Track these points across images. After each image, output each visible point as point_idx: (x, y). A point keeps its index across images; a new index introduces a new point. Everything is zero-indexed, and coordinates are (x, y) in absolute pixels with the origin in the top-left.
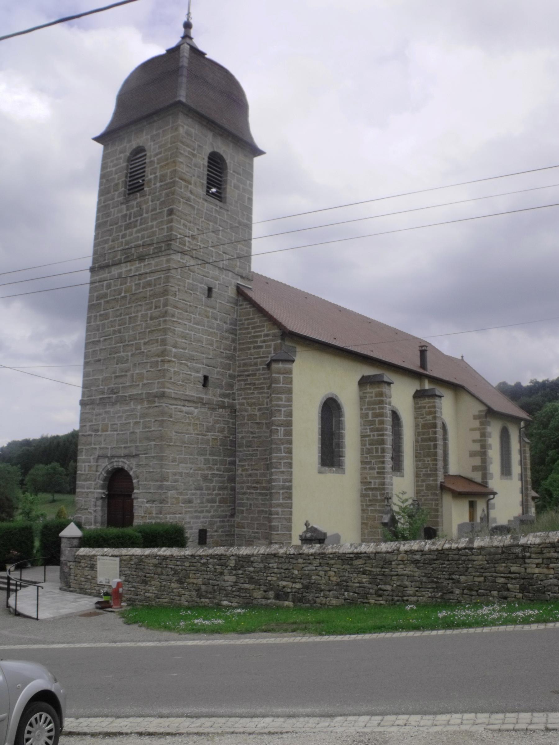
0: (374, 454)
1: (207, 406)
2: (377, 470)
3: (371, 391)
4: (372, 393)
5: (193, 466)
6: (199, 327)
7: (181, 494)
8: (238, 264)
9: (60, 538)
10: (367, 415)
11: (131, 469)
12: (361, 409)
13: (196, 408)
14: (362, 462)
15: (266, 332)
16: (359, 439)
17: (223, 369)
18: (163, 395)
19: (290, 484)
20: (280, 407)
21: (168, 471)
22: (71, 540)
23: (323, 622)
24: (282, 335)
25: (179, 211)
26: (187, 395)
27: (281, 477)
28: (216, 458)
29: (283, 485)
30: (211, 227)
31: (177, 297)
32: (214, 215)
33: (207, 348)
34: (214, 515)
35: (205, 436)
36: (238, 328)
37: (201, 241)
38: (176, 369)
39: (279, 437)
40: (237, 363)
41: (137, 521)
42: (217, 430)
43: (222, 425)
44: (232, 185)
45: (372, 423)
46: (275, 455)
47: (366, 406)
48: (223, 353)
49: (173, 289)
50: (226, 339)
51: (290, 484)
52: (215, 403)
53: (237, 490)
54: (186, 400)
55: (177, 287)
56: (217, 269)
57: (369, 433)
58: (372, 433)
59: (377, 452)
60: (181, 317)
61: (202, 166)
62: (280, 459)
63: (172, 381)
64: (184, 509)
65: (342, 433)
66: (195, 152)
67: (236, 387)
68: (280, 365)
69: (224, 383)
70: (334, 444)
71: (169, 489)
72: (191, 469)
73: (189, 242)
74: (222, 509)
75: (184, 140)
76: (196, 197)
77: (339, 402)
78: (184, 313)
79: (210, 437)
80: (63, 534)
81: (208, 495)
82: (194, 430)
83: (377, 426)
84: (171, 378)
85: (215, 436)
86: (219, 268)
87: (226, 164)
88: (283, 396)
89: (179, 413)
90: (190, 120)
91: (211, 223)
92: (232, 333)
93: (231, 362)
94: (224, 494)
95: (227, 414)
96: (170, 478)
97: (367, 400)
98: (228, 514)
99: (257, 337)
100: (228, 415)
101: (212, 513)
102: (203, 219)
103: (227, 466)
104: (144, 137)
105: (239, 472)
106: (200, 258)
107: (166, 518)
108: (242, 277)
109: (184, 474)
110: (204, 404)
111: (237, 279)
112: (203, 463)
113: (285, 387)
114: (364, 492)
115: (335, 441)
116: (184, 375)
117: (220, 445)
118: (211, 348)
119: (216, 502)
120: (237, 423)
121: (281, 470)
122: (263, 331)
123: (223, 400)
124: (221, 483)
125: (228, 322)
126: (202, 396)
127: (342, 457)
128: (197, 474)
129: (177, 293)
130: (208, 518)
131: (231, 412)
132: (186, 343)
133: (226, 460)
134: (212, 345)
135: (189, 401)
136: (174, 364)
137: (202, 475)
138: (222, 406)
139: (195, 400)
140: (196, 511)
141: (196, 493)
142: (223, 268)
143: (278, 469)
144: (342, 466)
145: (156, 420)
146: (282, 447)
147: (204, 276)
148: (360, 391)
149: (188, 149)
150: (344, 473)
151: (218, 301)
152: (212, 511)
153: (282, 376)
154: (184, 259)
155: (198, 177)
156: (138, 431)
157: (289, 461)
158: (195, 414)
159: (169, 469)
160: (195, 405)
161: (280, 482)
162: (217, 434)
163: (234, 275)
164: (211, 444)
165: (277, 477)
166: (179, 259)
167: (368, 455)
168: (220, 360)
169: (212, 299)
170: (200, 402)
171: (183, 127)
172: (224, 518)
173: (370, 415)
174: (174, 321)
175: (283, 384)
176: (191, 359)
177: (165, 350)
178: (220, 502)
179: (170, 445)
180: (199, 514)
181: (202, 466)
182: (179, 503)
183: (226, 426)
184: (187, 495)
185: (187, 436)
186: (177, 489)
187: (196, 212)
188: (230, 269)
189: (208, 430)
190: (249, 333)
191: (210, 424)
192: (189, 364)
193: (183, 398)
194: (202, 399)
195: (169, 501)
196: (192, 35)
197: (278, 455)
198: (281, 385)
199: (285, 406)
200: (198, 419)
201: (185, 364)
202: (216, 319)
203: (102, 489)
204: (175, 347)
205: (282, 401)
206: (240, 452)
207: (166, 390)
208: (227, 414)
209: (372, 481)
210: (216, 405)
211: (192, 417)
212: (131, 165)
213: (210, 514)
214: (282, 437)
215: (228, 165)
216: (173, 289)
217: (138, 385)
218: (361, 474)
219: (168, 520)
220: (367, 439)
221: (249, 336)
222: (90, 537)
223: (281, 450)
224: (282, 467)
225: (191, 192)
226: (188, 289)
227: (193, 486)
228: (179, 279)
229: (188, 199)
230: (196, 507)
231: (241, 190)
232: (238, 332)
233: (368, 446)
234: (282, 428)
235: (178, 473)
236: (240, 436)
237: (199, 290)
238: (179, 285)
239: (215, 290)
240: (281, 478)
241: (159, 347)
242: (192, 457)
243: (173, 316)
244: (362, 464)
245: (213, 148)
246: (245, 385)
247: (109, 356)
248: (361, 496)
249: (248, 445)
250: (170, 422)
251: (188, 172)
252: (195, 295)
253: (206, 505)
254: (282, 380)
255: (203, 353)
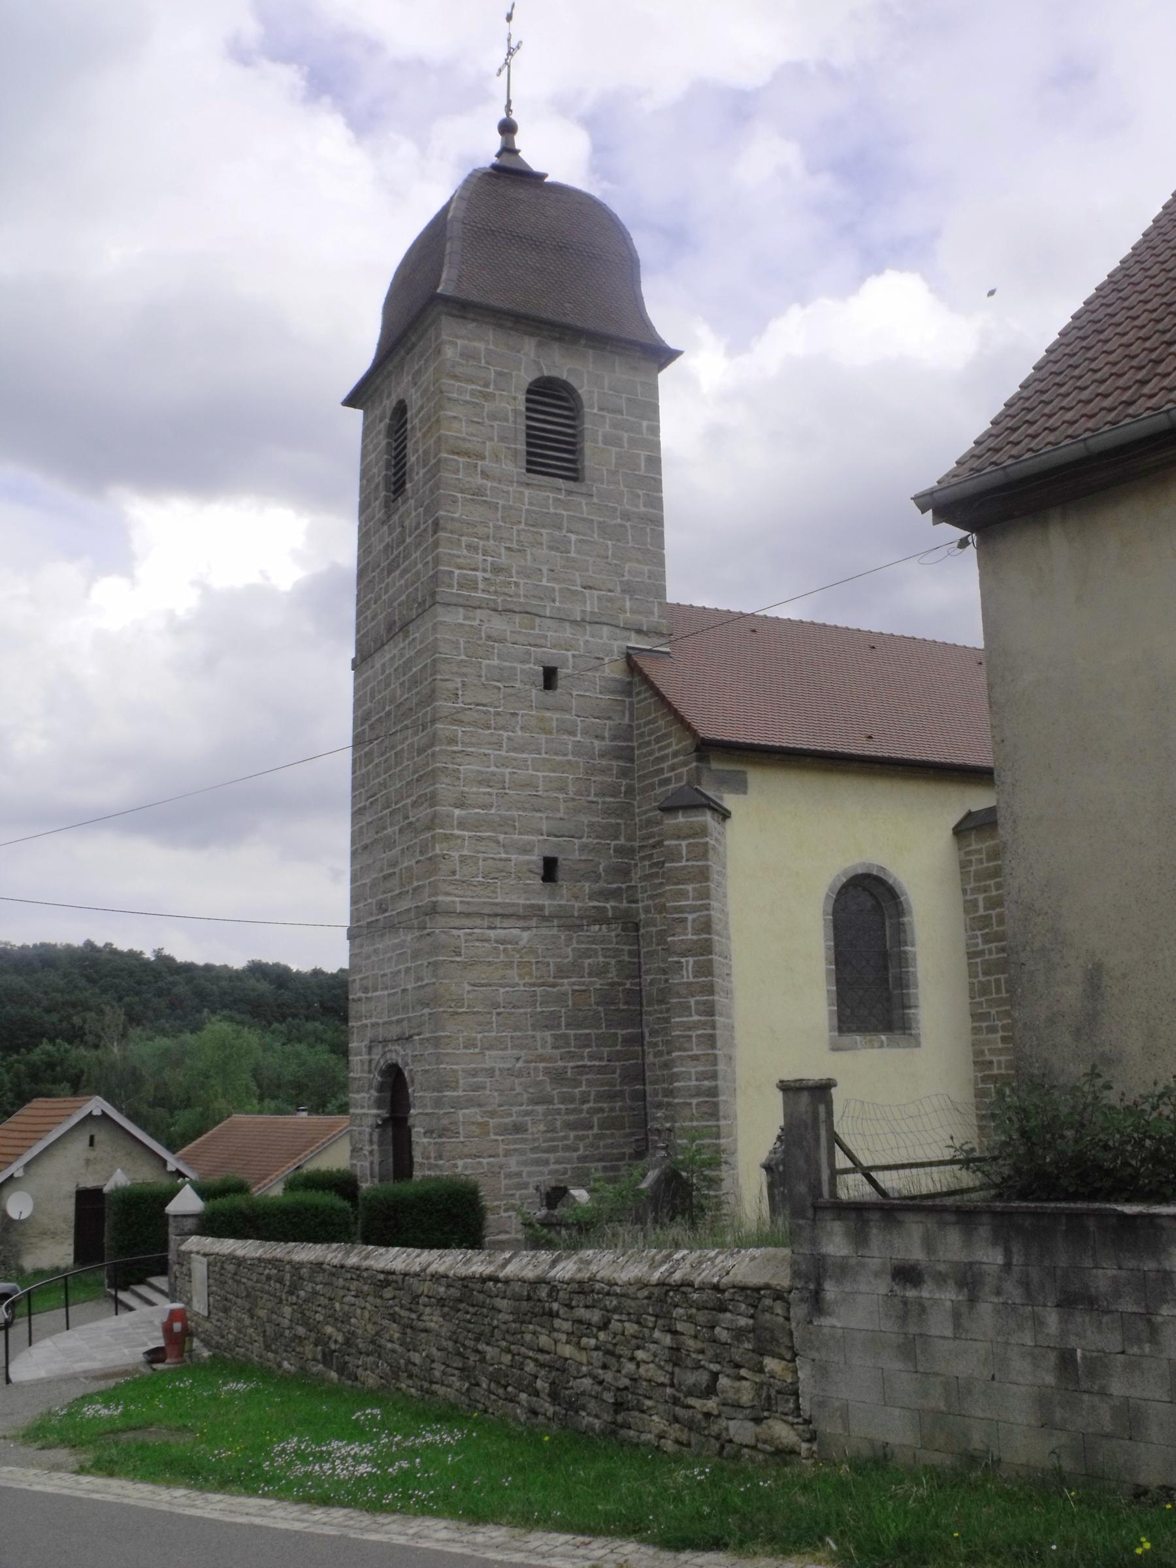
0: (994, 996)
1: (556, 922)
2: (1001, 1033)
3: (979, 845)
4: (979, 851)
5: (523, 1053)
6: (524, 756)
7: (492, 1114)
8: (628, 604)
9: (168, 1215)
10: (975, 903)
11: (407, 1064)
12: (964, 891)
13: (524, 929)
14: (975, 1017)
15: (675, 748)
16: (965, 960)
17: (597, 837)
18: (433, 910)
19: (713, 1083)
20: (682, 912)
21: (455, 1067)
22: (179, 1219)
23: (178, 1429)
24: (697, 750)
25: (453, 519)
26: (496, 904)
27: (694, 1069)
28: (587, 1031)
29: (697, 1087)
30: (545, 539)
31: (460, 700)
32: (552, 510)
33: (548, 797)
34: (586, 1157)
35: (554, 985)
36: (635, 744)
37: (518, 573)
38: (465, 852)
39: (685, 980)
40: (637, 819)
41: (417, 1174)
42: (587, 971)
43: (601, 959)
44: (600, 438)
45: (985, 921)
46: (678, 1019)
47: (972, 885)
48: (596, 803)
49: (450, 685)
50: (603, 771)
51: (713, 1083)
52: (576, 914)
53: (649, 1099)
54: (496, 915)
55: (458, 680)
56: (567, 625)
57: (981, 947)
58: (986, 947)
59: (998, 990)
60: (474, 740)
61: (510, 415)
62: (690, 1029)
63: (457, 877)
64: (502, 1146)
65: (905, 952)
66: (491, 389)
67: (636, 875)
68: (681, 819)
69: (601, 868)
70: (890, 980)
71: (457, 1104)
72: (518, 1059)
73: (485, 579)
74: (610, 1141)
75: (459, 370)
76: (500, 481)
77: (890, 882)
78: (480, 731)
79: (566, 988)
80: (172, 1208)
81: (566, 1113)
82: (521, 976)
83: (996, 928)
84: (454, 873)
85: (583, 984)
86: (574, 622)
87: (579, 396)
88: (690, 887)
89: (477, 944)
90: (472, 326)
91: (544, 531)
92: (618, 758)
93: (619, 821)
94: (612, 1109)
95: (613, 934)
96: (461, 1082)
97: (973, 869)
98: (628, 1150)
99: (663, 759)
100: (617, 936)
101: (581, 1152)
102: (522, 526)
103: (618, 1048)
104: (405, 380)
105: (650, 1059)
106: (517, 609)
107: (455, 1166)
108: (639, 631)
109: (497, 1073)
110: (544, 918)
111: (629, 639)
112: (549, 1046)
113: (693, 866)
114: (980, 1086)
115: (892, 972)
116: (490, 862)
117: (598, 1004)
118: (561, 796)
119: (591, 1128)
120: (643, 951)
121: (690, 1053)
122: (669, 745)
123: (602, 904)
124: (602, 1085)
125: (607, 735)
126: (540, 902)
127: (909, 1007)
128: (536, 1069)
129: (460, 693)
130: (569, 1161)
131: (623, 930)
132: (490, 794)
133: (616, 1034)
134: (562, 789)
135: (503, 916)
136: (459, 841)
137: (547, 1071)
138: (600, 918)
139: (521, 911)
140: (533, 1150)
141: (532, 1111)
142: (583, 620)
143: (685, 1050)
144: (910, 1028)
145: (429, 963)
146: (692, 1001)
147: (530, 645)
148: (959, 849)
149: (471, 387)
150: (918, 1044)
151: (575, 693)
152: (581, 1146)
153: (684, 843)
154: (474, 619)
155: (502, 439)
156: (409, 987)
157: (709, 1032)
158: (522, 943)
159: (457, 1064)
160: (521, 923)
161: (690, 1079)
162: (587, 980)
163: (617, 631)
164: (570, 1003)
165: (683, 1069)
166: (461, 621)
167: (983, 999)
168: (585, 819)
169: (559, 691)
170: (534, 913)
171: (454, 344)
172: (617, 1160)
173: (981, 904)
174: (455, 752)
175: (688, 860)
176: (506, 824)
177: (435, 816)
178: (602, 1126)
179: (457, 1013)
180: (545, 1155)
181: (549, 1051)
182: (488, 1134)
183: (613, 961)
184: (511, 1115)
185: (502, 990)
186: (480, 1105)
187: (500, 515)
188: (604, 619)
189: (561, 972)
190: (651, 753)
191: (566, 961)
192: (501, 837)
193: (486, 911)
194: (541, 908)
195: (461, 1130)
196: (518, 145)
197: (684, 1019)
198: (684, 863)
199: (694, 909)
200: (532, 951)
201: (489, 838)
202: (573, 733)
203: (379, 1108)
204: (461, 805)
205: (687, 899)
206: (649, 1013)
207: (440, 898)
208: (613, 934)
209: (995, 1059)
210: (581, 917)
211: (513, 950)
212: (396, 441)
213: (575, 1155)
214: (691, 979)
215: (584, 397)
216: (450, 685)
217: (408, 892)
218: (973, 1045)
219: (459, 1170)
220: (979, 960)
221: (651, 758)
222: (213, 1213)
223: (689, 1007)
224: (695, 1047)
225: (485, 475)
226: (487, 679)
227: (525, 1096)
228: (462, 661)
229: (479, 492)
230: (534, 1140)
231: (626, 445)
232: (637, 752)
233: (982, 978)
234: (691, 960)
235: (482, 1069)
236: (649, 978)
237: (519, 677)
238: (465, 675)
239: (562, 672)
240: (693, 1070)
241: (429, 811)
242: (518, 1034)
243: (452, 741)
244: (973, 1021)
245: (541, 369)
246: (651, 866)
247: (376, 837)
248: (976, 1096)
249: (660, 998)
250: (453, 965)
251: (472, 435)
252: (509, 690)
253: (562, 1134)
254: (684, 852)
255: (539, 811)
